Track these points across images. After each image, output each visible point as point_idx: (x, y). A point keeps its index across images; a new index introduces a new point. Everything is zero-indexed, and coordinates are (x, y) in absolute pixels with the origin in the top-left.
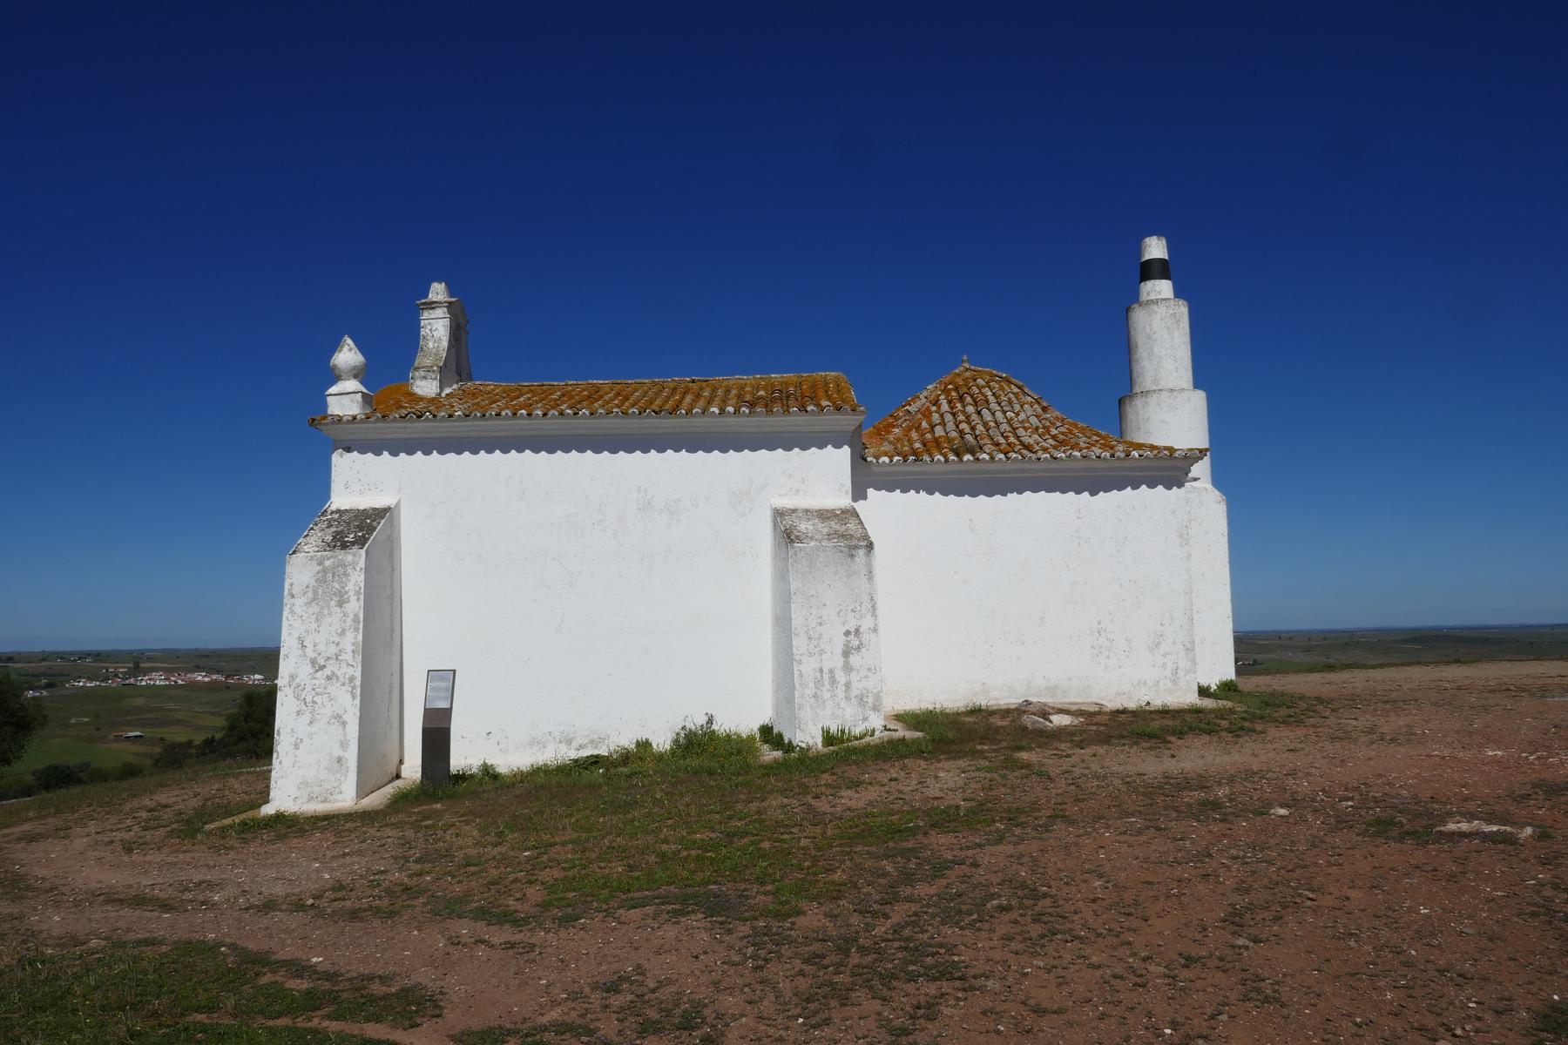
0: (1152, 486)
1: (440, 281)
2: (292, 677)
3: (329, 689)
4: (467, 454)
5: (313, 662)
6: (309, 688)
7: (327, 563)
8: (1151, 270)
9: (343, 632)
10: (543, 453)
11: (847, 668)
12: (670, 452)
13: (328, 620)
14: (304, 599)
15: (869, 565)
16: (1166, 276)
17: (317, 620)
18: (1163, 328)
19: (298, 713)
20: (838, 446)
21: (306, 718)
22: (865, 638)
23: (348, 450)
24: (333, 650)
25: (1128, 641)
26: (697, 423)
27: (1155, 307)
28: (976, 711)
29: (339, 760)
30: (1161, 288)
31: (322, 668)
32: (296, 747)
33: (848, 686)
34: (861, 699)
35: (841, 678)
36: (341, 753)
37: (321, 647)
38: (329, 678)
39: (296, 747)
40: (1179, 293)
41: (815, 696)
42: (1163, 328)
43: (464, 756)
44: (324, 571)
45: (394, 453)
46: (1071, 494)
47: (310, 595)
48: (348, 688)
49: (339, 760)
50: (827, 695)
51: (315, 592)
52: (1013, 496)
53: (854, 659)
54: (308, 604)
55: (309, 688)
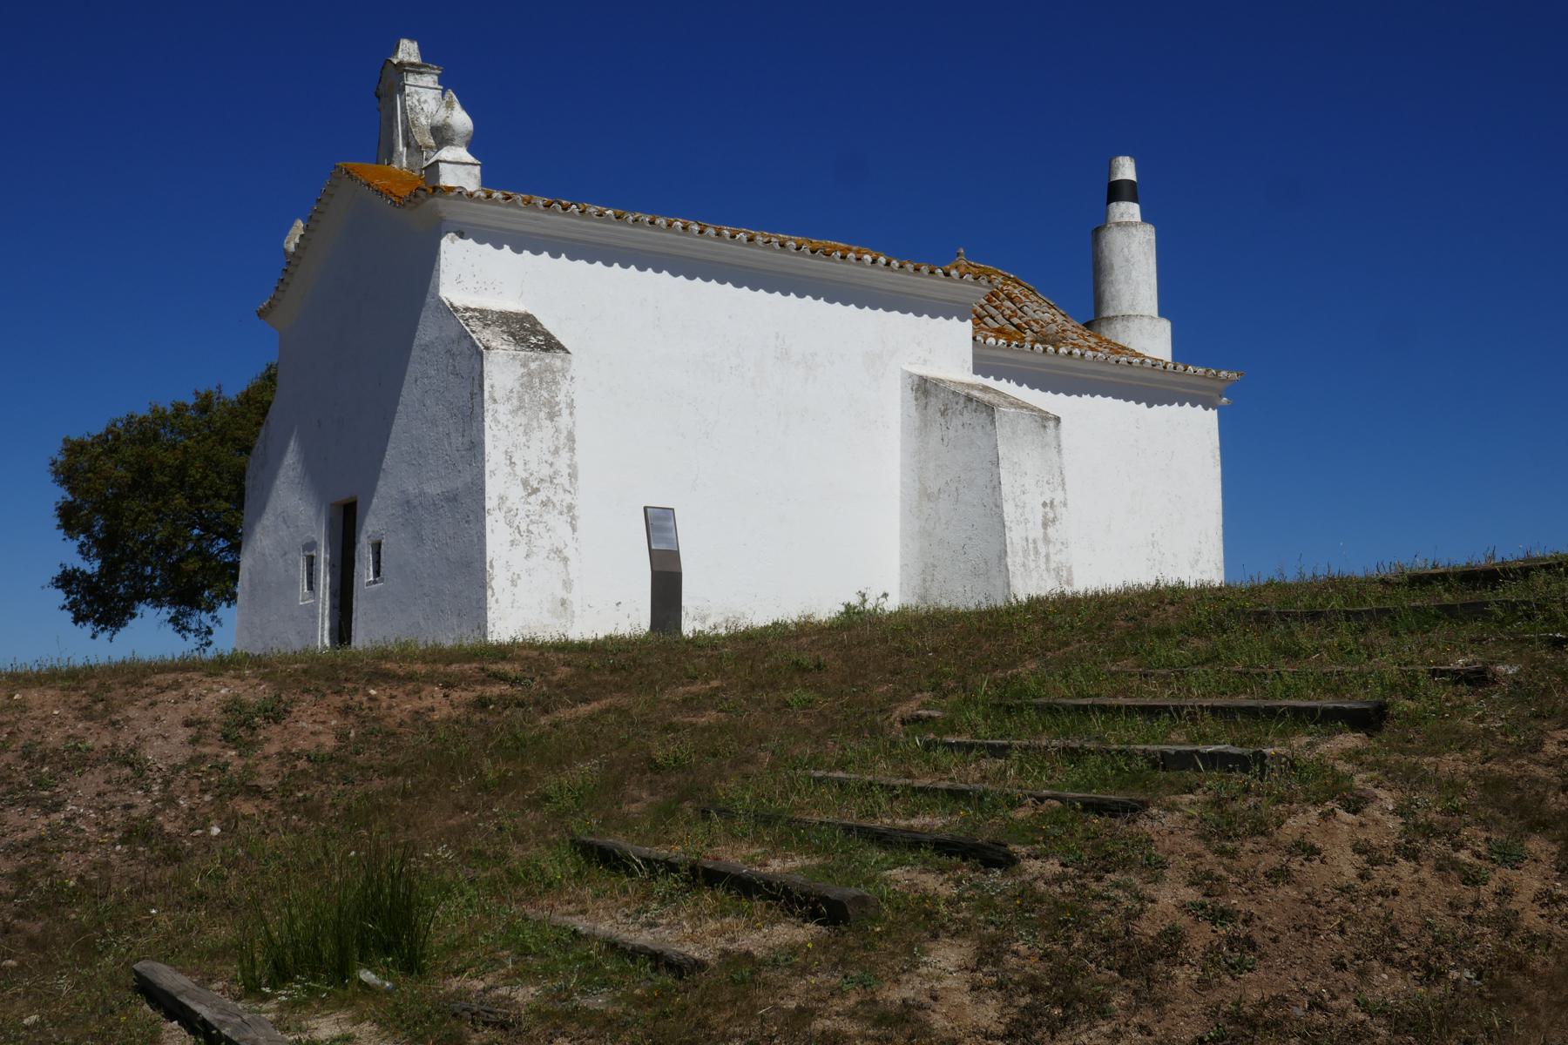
0: (1194, 405)
1: (411, 39)
2: (502, 499)
3: (546, 517)
4: (599, 264)
5: (525, 483)
6: (522, 514)
7: (533, 366)
8: (1117, 191)
9: (556, 452)
10: (682, 278)
11: (1047, 540)
12: (809, 298)
13: (537, 435)
14: (508, 407)
15: (1057, 437)
16: (1135, 200)
17: (526, 433)
18: (1133, 251)
19: (512, 543)
20: (963, 319)
21: (522, 550)
22: (1060, 510)
23: (462, 235)
24: (546, 471)
25: (1175, 555)
26: (833, 268)
27: (1134, 230)
28: (1127, 591)
29: (563, 603)
30: (1129, 211)
31: (536, 491)
32: (514, 583)
33: (1047, 556)
34: (1058, 571)
35: (1042, 549)
36: (564, 594)
37: (533, 466)
38: (544, 504)
39: (514, 583)
40: (1146, 218)
41: (1024, 565)
42: (1133, 251)
43: (707, 608)
44: (530, 374)
45: (517, 249)
46: (1132, 403)
47: (515, 402)
48: (565, 517)
49: (563, 603)
50: (1033, 565)
51: (521, 399)
52: (1086, 398)
53: (1050, 530)
54: (514, 412)
55: (522, 514)
